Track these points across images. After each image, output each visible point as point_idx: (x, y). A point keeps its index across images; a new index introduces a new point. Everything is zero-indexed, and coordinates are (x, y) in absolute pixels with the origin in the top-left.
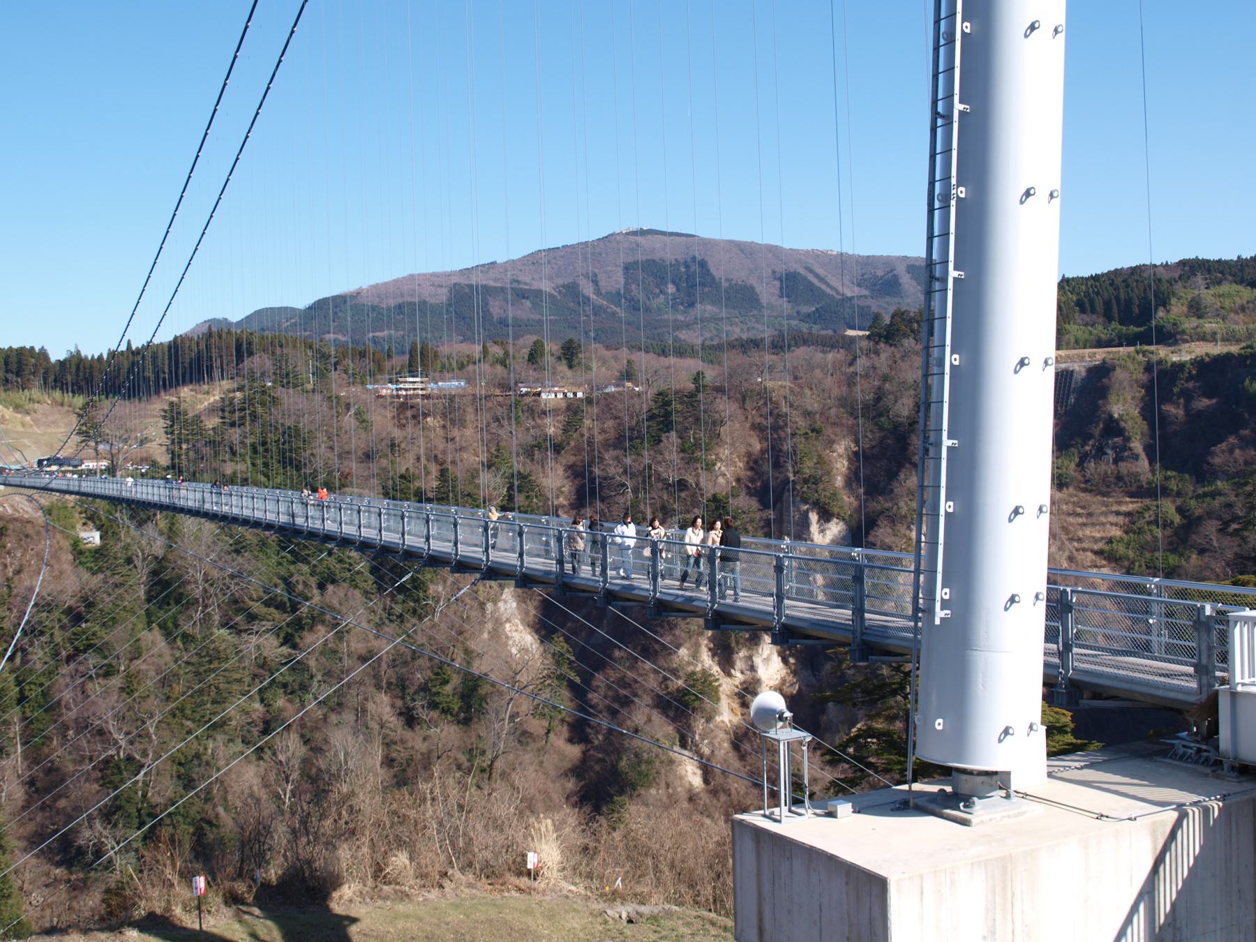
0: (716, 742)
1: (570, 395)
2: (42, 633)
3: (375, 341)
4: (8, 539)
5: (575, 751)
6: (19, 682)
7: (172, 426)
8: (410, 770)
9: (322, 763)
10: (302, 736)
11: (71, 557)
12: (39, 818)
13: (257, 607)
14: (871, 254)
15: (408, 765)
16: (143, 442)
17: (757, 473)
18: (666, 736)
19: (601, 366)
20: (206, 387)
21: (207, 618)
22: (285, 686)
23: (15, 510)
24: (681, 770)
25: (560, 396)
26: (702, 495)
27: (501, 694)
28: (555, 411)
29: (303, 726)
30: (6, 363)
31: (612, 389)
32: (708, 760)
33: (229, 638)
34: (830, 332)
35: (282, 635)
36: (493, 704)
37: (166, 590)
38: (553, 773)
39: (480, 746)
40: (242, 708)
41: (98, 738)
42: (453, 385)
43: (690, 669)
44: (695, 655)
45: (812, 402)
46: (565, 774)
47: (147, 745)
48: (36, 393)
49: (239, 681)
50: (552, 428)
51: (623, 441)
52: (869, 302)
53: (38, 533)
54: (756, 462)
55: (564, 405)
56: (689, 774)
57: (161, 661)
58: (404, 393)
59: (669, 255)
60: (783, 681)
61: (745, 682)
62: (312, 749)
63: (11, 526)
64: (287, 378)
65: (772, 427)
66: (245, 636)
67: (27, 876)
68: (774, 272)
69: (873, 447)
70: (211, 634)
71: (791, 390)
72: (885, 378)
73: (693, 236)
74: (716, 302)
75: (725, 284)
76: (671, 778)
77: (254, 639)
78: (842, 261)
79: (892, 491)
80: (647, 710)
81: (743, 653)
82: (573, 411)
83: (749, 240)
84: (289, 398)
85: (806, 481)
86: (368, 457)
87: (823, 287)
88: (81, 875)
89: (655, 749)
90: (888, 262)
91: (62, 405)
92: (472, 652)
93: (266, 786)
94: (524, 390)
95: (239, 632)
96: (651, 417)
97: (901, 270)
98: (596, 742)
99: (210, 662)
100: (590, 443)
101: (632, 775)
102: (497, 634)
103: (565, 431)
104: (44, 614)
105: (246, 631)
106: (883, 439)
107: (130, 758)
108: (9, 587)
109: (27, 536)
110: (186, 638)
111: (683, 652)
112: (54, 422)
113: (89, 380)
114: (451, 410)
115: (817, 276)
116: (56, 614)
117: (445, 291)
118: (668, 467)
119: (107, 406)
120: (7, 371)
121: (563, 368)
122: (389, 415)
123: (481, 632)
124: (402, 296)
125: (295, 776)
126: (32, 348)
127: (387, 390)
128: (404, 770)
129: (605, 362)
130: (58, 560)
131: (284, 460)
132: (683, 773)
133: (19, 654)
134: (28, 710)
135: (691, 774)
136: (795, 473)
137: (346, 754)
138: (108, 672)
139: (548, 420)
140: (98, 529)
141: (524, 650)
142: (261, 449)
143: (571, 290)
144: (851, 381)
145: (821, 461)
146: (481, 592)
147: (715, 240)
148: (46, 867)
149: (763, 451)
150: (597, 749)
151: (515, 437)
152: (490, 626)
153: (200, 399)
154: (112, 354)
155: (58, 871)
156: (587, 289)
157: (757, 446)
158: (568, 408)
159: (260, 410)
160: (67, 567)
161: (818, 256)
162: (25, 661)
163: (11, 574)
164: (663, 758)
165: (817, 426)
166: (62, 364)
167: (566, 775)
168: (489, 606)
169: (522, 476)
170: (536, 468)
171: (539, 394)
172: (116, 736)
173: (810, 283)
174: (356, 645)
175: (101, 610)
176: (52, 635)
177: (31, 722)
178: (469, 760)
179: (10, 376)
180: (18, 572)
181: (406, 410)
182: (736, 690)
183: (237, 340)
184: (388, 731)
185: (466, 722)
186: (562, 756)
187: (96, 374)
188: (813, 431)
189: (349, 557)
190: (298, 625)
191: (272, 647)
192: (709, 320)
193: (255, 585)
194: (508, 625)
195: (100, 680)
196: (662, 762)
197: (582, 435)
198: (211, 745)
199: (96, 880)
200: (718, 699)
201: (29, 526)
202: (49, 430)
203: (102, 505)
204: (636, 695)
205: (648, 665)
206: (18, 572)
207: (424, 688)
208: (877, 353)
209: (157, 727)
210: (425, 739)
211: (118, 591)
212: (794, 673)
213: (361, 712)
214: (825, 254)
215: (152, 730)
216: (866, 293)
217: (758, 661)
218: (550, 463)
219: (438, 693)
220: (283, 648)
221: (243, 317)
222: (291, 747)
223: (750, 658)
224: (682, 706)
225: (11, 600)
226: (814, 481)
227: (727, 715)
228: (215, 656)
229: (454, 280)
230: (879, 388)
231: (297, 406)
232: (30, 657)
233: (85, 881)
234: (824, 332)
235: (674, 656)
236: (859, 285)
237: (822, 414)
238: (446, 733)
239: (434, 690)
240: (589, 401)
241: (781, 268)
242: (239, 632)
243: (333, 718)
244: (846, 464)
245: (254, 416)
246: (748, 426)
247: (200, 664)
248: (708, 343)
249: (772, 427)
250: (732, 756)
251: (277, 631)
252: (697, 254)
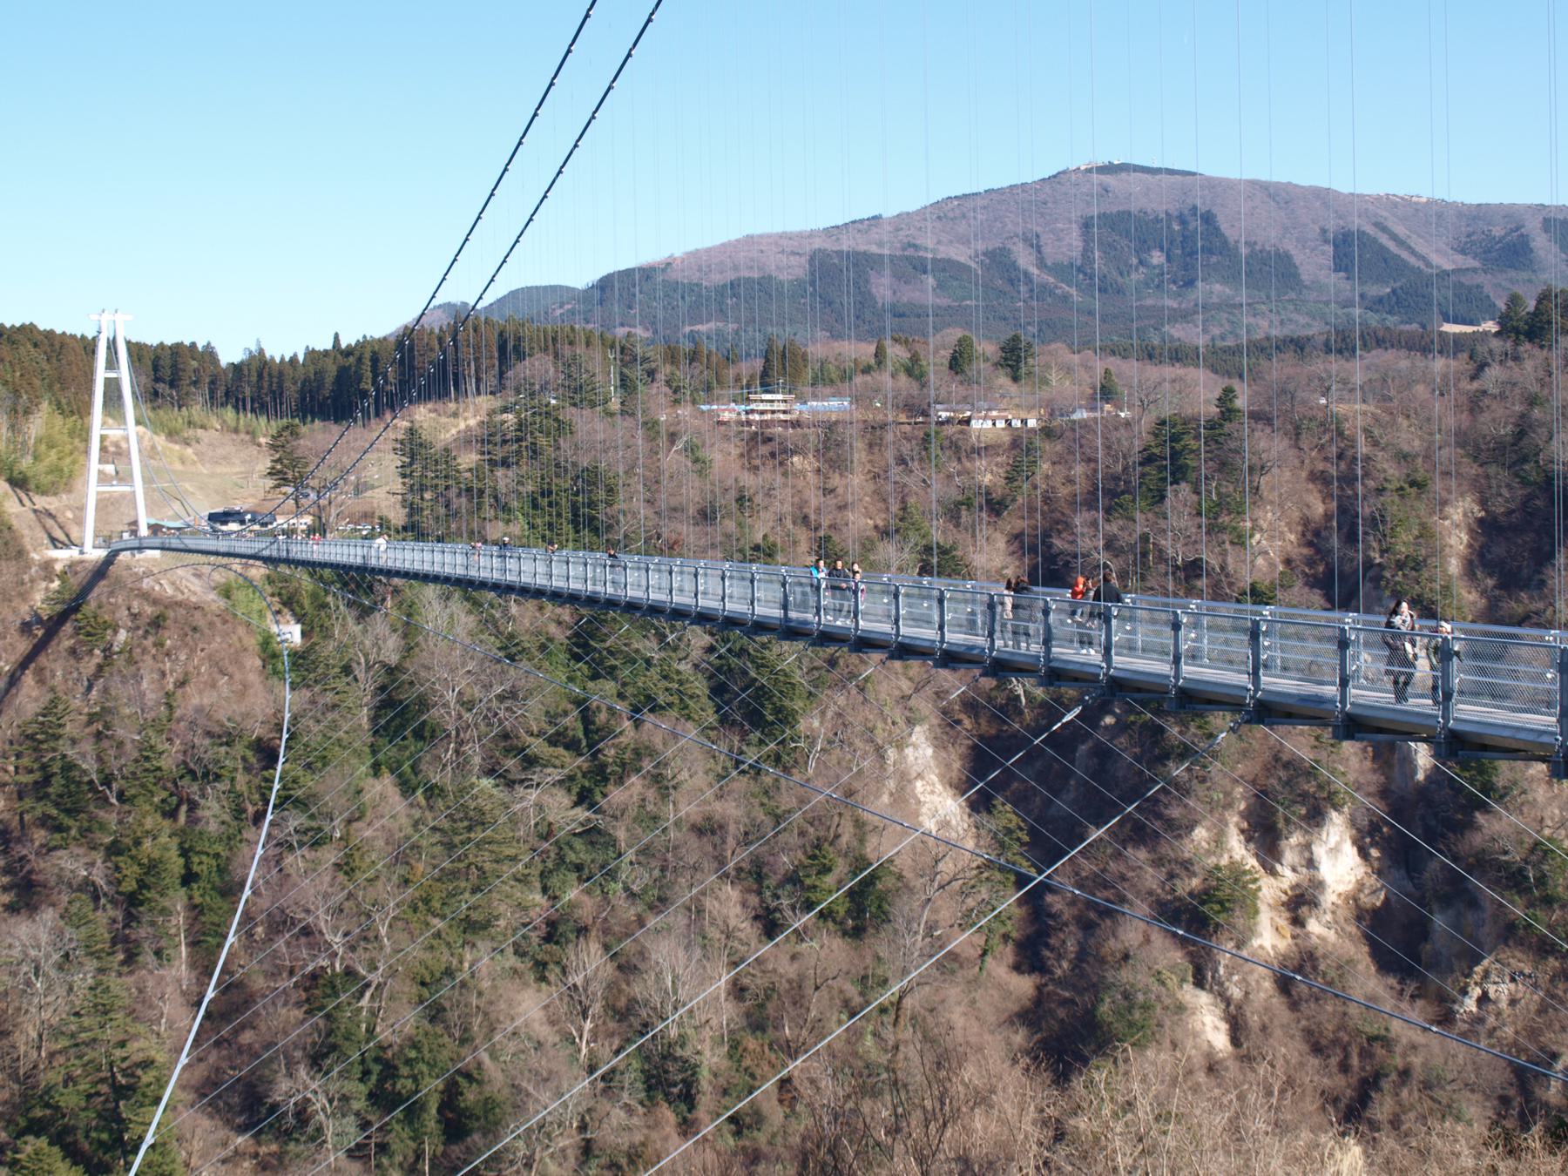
0: (1252, 979)
1: (1017, 423)
2: (218, 777)
3: (692, 337)
4: (167, 633)
5: (1024, 985)
6: (185, 853)
7: (411, 464)
8: (770, 1008)
9: (637, 990)
10: (607, 948)
11: (259, 663)
12: (212, 1058)
13: (537, 746)
14: (1483, 201)
15: (768, 997)
16: (359, 489)
17: (1318, 551)
18: (1172, 968)
19: (1067, 376)
20: (452, 406)
21: (462, 766)
22: (579, 868)
23: (177, 589)
24: (1194, 1022)
25: (1001, 424)
26: (1231, 585)
27: (911, 890)
28: (989, 450)
29: (606, 931)
30: (156, 368)
31: (1081, 415)
32: (1239, 1007)
33: (495, 791)
34: (1415, 326)
35: (575, 790)
36: (901, 908)
37: (401, 715)
38: (992, 1019)
39: (879, 972)
40: (519, 904)
41: (303, 940)
42: (832, 406)
43: (1212, 861)
44: (1219, 841)
45: (1408, 437)
46: (1010, 1022)
47: (375, 953)
48: (197, 410)
49: (514, 859)
50: (988, 475)
51: (1111, 495)
52: (1480, 279)
53: (211, 624)
54: (1317, 533)
55: (1007, 439)
56: (1208, 1028)
57: (395, 826)
58: (757, 417)
59: (1160, 203)
60: (1360, 886)
61: (1298, 885)
62: (620, 968)
63: (171, 614)
64: (580, 393)
65: (1342, 477)
66: (520, 790)
67: (197, 1145)
68: (1324, 231)
69: (1512, 512)
70: (472, 786)
71: (1376, 419)
72: (1532, 401)
73: (1194, 174)
74: (1232, 277)
75: (1244, 251)
76: (1179, 1035)
77: (533, 795)
78: (1434, 214)
79: (1542, 583)
80: (1142, 925)
81: (1295, 839)
82: (1020, 447)
83: (1284, 180)
84: (587, 424)
85: (1400, 565)
86: (706, 515)
87: (1405, 255)
88: (274, 1147)
89: (1155, 987)
90: (1510, 214)
91: (236, 431)
92: (864, 824)
93: (552, 1023)
94: (944, 415)
95: (510, 784)
96: (1148, 459)
97: (1533, 226)
98: (1059, 972)
99: (470, 829)
100: (1047, 500)
101: (1119, 1027)
102: (902, 796)
103: (1010, 480)
104: (223, 749)
105: (522, 781)
106: (1529, 498)
107: (349, 973)
108: (170, 707)
109: (195, 629)
110: (433, 792)
111: (1200, 834)
112: (225, 458)
113: (278, 394)
114: (830, 445)
115: (1394, 237)
116: (239, 749)
117: (804, 260)
118: (1175, 539)
119: (316, 435)
120: (157, 380)
121: (1003, 380)
122: (735, 452)
123: (878, 796)
124: (736, 268)
125: (596, 1008)
126: (193, 345)
127: (729, 412)
128: (762, 1006)
129: (1069, 370)
130: (241, 667)
131: (578, 513)
132: (1198, 1026)
133: (184, 808)
134: (196, 894)
135: (1212, 1030)
136: (1383, 552)
137: (675, 978)
138: (317, 840)
139: (981, 463)
140: (298, 621)
141: (945, 824)
142: (544, 502)
143: (998, 260)
144: (1475, 404)
145: (1426, 533)
146: (879, 731)
147: (1228, 180)
148: (223, 1133)
149: (1328, 517)
150: (1059, 982)
151: (933, 487)
152: (891, 784)
153: (451, 424)
154: (311, 354)
155: (240, 1140)
156: (1024, 259)
157: (1319, 509)
158: (1015, 444)
159: (542, 441)
160: (254, 678)
161: (1395, 205)
162: (193, 820)
163: (171, 687)
164: (1167, 1001)
165: (1419, 477)
166: (237, 368)
167: (1012, 1023)
168: (891, 754)
169: (944, 552)
170: (963, 537)
171: (967, 421)
172: (327, 937)
173: (1382, 247)
174: (687, 808)
175: (306, 745)
176: (233, 780)
177: (201, 913)
178: (862, 994)
179: (161, 387)
180: (182, 684)
181: (763, 445)
182: (1284, 898)
183: (501, 335)
184: (736, 944)
185: (857, 933)
186: (1007, 994)
187: (287, 384)
188: (1413, 484)
189: (678, 672)
190: (600, 775)
191: (564, 812)
192: (1218, 307)
193: (533, 713)
194: (919, 784)
195: (305, 851)
196: (1166, 1008)
197: (1035, 487)
198: (468, 957)
199: (298, 1156)
200: (1257, 912)
201: (198, 614)
202: (219, 470)
203: (305, 581)
204: (1122, 900)
205: (1143, 854)
206: (182, 684)
207: (793, 879)
208: (1517, 359)
209: (390, 926)
210: (794, 957)
211: (330, 716)
212: (1379, 873)
213: (697, 911)
214: (1407, 202)
215: (383, 931)
216: (1475, 264)
217: (1320, 851)
218: (984, 531)
219: (815, 887)
220: (578, 810)
221: (506, 293)
222: (589, 962)
223: (1307, 847)
224: (1200, 918)
225: (173, 725)
226: (1415, 564)
227: (1269, 937)
228: (478, 820)
229: (818, 244)
230: (1523, 416)
231: (595, 435)
232: (200, 813)
233: (280, 1156)
234: (1407, 327)
235: (1186, 841)
236: (1463, 252)
237: (1426, 457)
238: (828, 951)
239: (808, 882)
240: (1047, 432)
241: (1332, 225)
242: (510, 784)
243: (652, 921)
244: (1465, 537)
245: (535, 452)
246: (1304, 474)
247: (455, 832)
248: (1219, 344)
249: (1342, 477)
250: (1278, 1002)
251: (566, 782)
252: (1199, 203)
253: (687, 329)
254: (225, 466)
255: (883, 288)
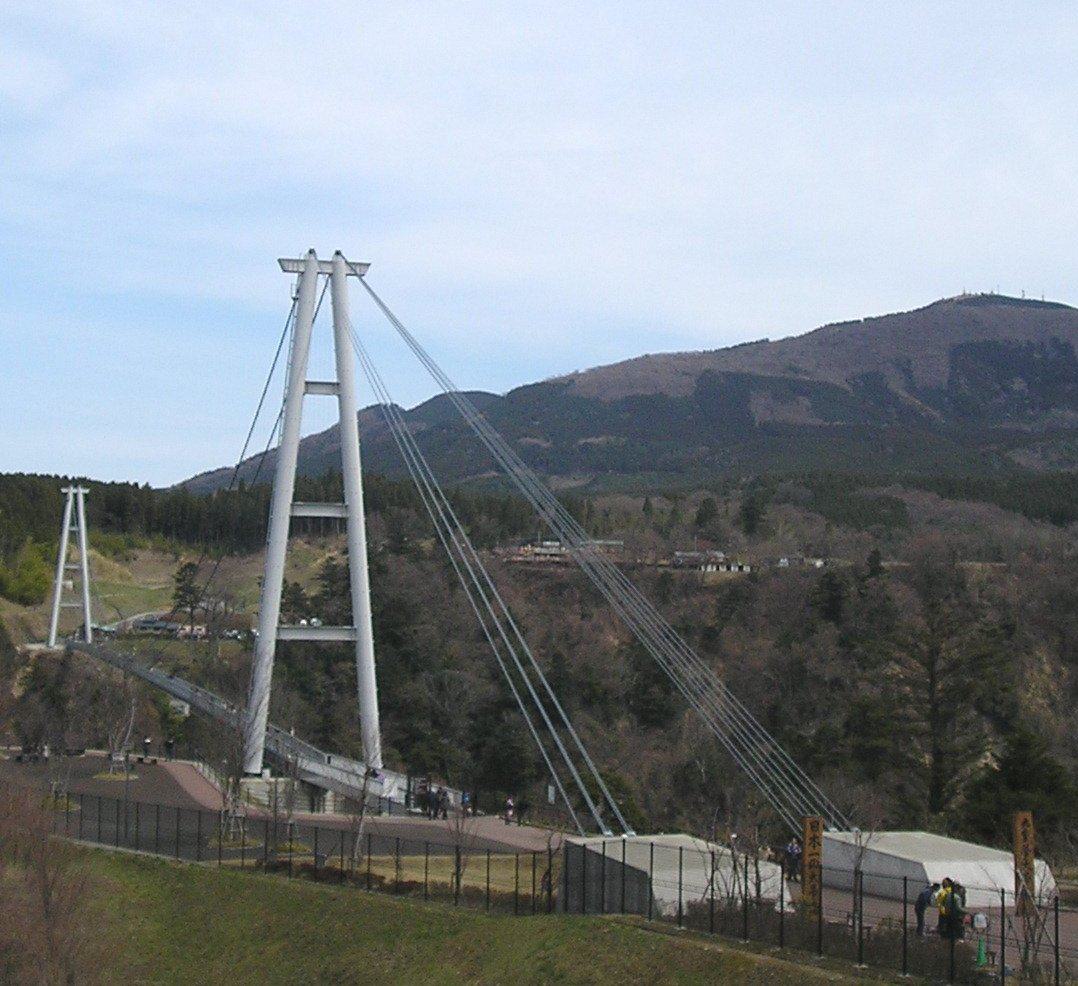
20: (321, 540)
126: (136, 484)
156: (896, 384)
253: (582, 442)
254: (149, 579)
255: (760, 408)
